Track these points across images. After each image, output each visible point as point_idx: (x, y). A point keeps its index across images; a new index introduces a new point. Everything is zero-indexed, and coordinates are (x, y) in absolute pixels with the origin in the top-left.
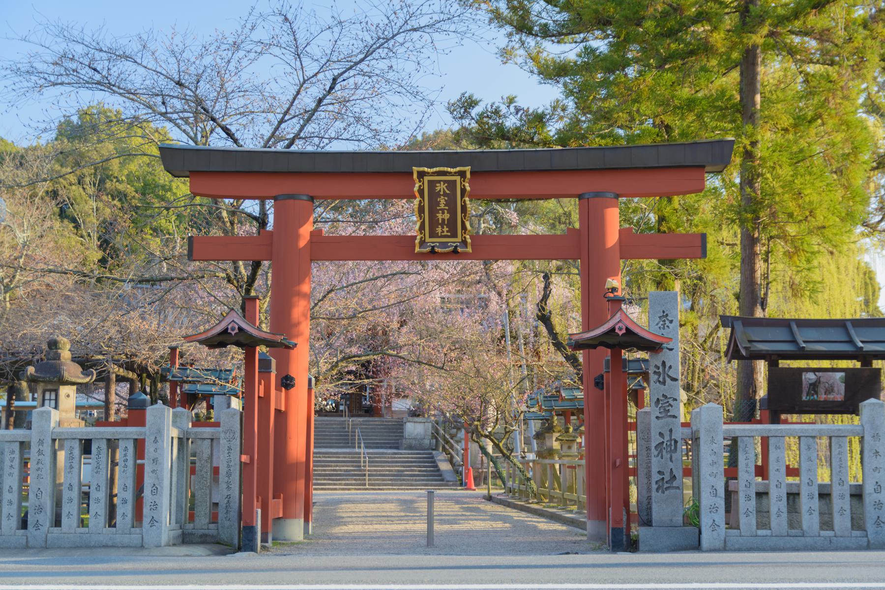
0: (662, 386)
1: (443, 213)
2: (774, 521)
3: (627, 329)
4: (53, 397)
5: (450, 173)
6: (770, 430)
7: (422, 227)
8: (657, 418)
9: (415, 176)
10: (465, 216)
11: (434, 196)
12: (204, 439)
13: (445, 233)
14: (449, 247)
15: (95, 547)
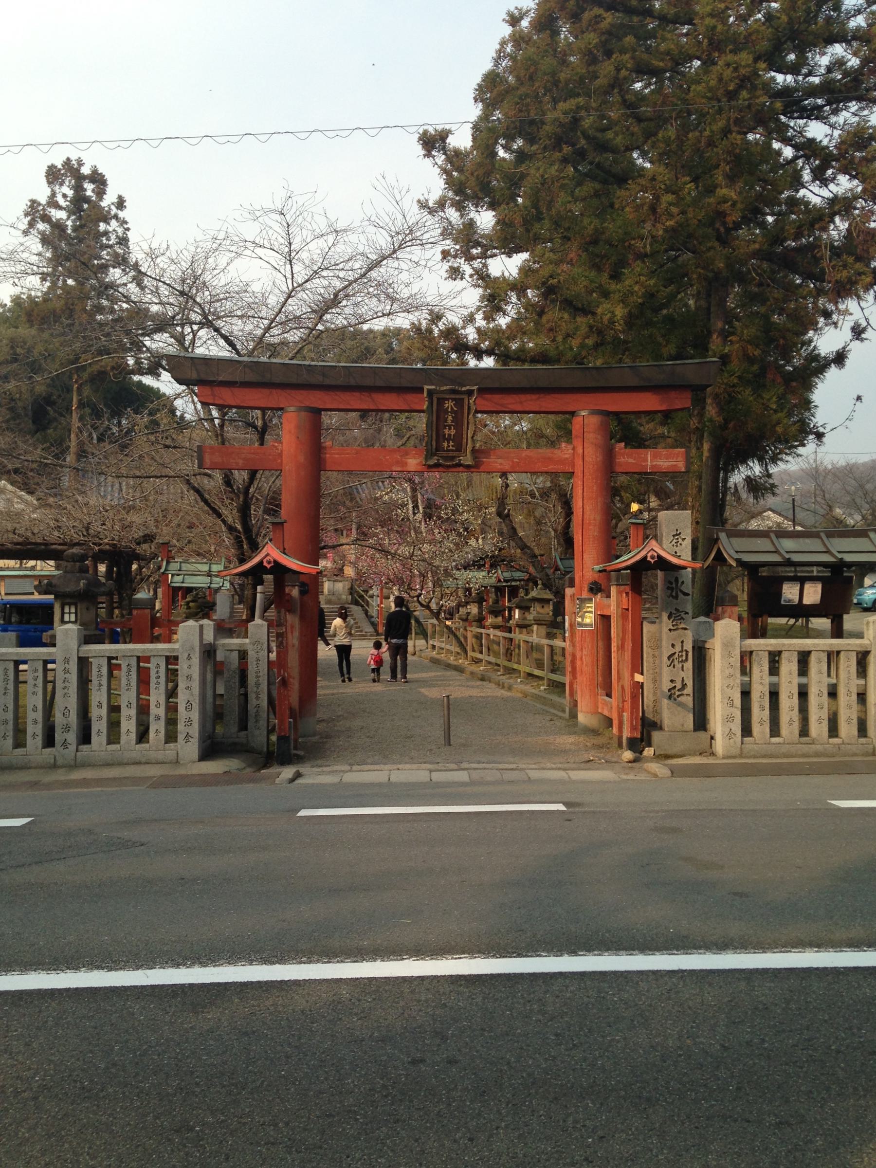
0: (675, 601)
1: (450, 429)
2: (784, 730)
3: (275, 561)
4: (73, 610)
6: (784, 645)
12: (232, 650)
15: (127, 764)
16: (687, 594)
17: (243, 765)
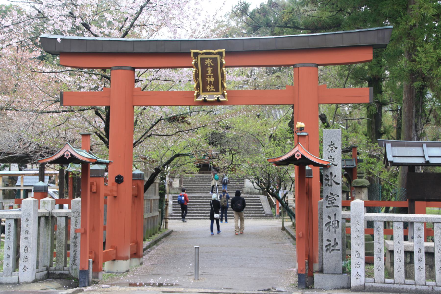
1: (210, 77)
3: (302, 156)
5: (213, 53)
6: (394, 217)
7: (198, 86)
8: (327, 207)
9: (192, 55)
10: (223, 79)
11: (204, 67)
12: (62, 216)
13: (212, 90)
14: (214, 98)
16: (338, 184)
17: (59, 285)
